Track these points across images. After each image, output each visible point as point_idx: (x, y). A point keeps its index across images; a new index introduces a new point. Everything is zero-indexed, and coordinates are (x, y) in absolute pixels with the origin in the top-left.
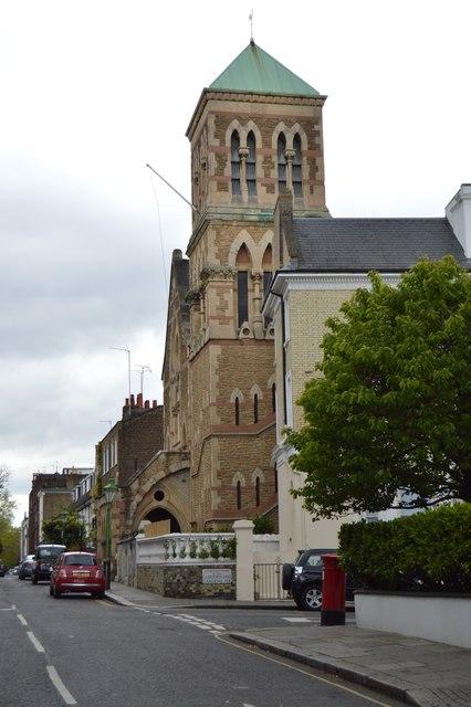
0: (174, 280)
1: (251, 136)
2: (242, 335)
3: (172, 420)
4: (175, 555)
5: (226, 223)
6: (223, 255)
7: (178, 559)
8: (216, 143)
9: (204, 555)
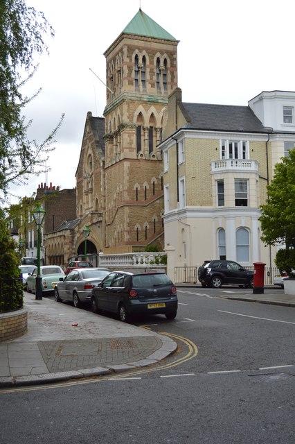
0: (88, 127)
1: (144, 59)
2: (139, 157)
3: (85, 197)
4: (137, 263)
5: (133, 101)
6: (130, 117)
7: (139, 265)
8: (128, 60)
9: (152, 263)
